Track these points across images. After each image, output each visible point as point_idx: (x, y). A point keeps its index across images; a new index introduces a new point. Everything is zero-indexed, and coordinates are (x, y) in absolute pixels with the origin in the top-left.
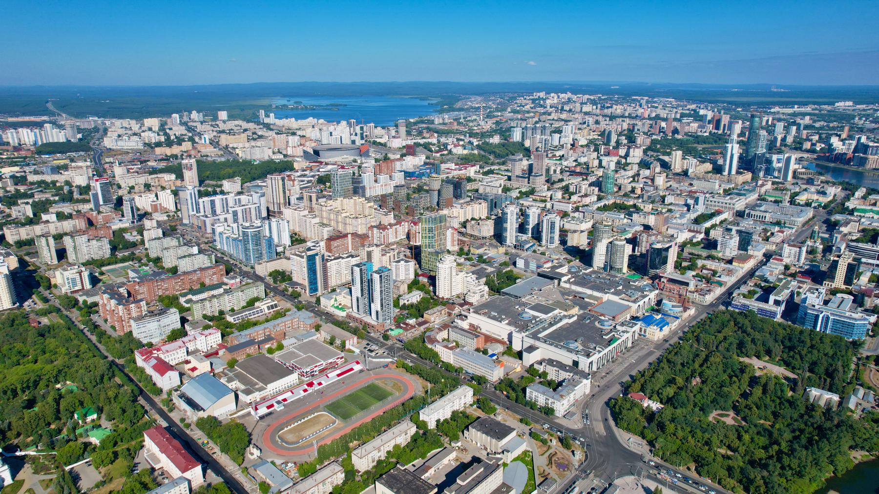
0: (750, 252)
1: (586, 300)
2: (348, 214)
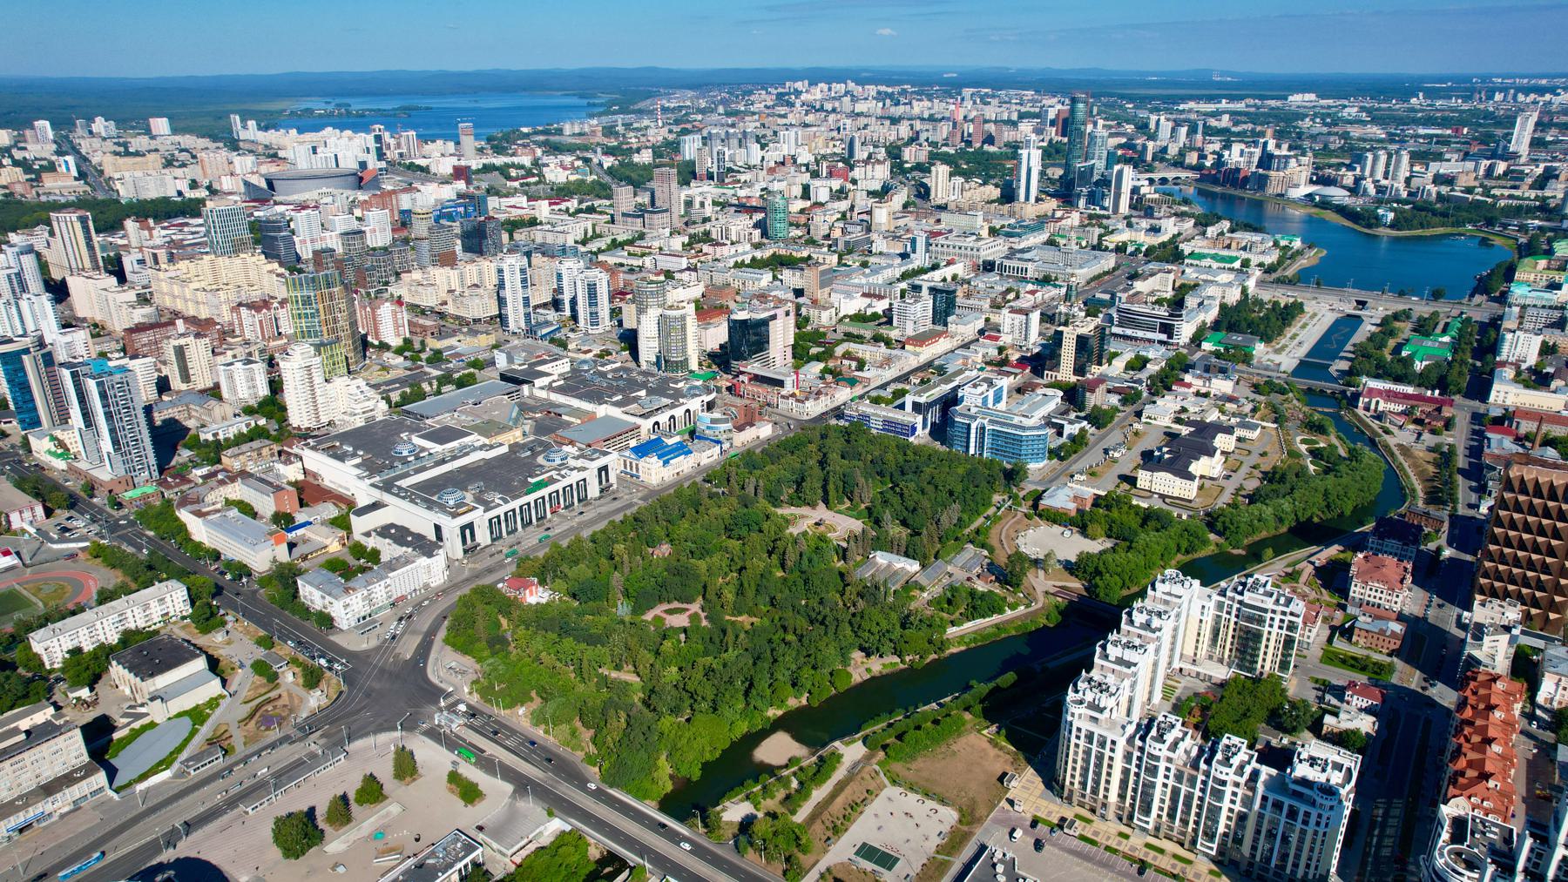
0: (952, 328)
1: (565, 417)
2: (203, 284)
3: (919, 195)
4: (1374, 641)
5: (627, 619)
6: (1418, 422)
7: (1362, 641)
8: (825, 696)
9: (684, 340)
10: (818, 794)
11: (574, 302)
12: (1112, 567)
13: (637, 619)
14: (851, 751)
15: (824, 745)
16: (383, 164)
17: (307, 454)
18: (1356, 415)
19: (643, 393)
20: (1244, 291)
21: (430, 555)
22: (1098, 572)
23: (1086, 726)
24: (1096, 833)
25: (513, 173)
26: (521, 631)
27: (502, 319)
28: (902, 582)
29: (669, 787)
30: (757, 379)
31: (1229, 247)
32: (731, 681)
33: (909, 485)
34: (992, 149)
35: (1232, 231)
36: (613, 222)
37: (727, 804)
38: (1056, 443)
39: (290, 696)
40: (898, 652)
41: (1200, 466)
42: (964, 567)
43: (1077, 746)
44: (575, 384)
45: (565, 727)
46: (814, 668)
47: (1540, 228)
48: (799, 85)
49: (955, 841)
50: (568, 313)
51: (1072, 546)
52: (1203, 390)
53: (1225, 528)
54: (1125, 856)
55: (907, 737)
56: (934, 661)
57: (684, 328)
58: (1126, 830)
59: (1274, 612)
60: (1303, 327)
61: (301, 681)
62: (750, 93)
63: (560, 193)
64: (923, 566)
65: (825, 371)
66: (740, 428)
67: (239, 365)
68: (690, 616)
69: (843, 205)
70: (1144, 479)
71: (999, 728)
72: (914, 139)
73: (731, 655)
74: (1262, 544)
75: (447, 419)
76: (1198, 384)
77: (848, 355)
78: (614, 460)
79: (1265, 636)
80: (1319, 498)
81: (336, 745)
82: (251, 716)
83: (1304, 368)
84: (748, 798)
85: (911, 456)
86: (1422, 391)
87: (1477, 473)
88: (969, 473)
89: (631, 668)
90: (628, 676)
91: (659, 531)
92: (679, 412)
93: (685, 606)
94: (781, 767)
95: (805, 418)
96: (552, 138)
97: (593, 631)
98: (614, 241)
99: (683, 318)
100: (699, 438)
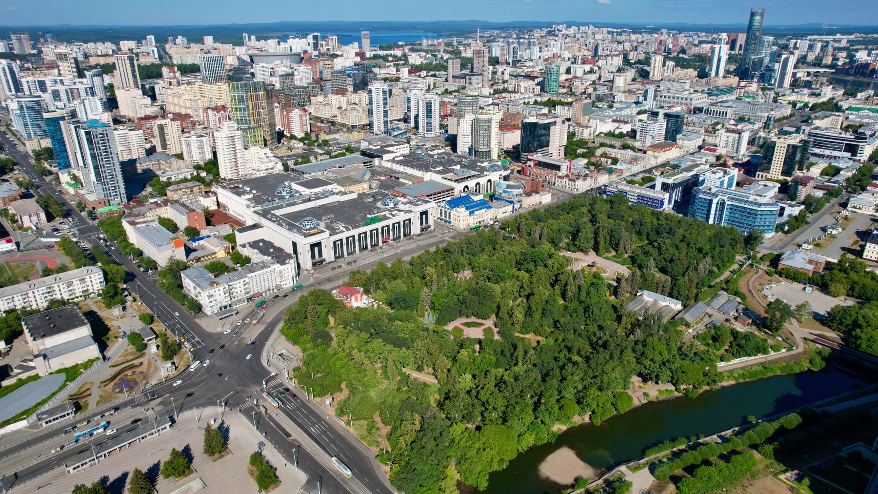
0: (679, 142)
1: (401, 180)
3: (641, 76)
5: (431, 327)
8: (608, 416)
9: (489, 137)
11: (417, 117)
15: (610, 468)
17: (220, 191)
19: (458, 167)
22: (856, 325)
25: (390, 59)
27: (370, 125)
30: (540, 164)
33: (667, 243)
36: (447, 80)
38: (779, 220)
39: (149, 364)
40: (675, 382)
42: (719, 309)
44: (410, 160)
46: (600, 389)
48: (560, 27)
50: (413, 124)
51: (823, 303)
56: (706, 392)
57: (489, 128)
61: (161, 353)
62: (532, 31)
63: (414, 70)
64: (685, 306)
65: (588, 164)
66: (528, 194)
67: (194, 138)
68: (484, 330)
69: (594, 77)
71: (799, 479)
73: (520, 369)
75: (319, 175)
77: (605, 155)
78: (432, 207)
82: (114, 377)
85: (663, 221)
88: (716, 235)
89: (431, 370)
90: (426, 377)
91: (463, 260)
92: (483, 181)
93: (480, 321)
95: (575, 193)
98: (446, 90)
99: (489, 121)
100: (497, 199)
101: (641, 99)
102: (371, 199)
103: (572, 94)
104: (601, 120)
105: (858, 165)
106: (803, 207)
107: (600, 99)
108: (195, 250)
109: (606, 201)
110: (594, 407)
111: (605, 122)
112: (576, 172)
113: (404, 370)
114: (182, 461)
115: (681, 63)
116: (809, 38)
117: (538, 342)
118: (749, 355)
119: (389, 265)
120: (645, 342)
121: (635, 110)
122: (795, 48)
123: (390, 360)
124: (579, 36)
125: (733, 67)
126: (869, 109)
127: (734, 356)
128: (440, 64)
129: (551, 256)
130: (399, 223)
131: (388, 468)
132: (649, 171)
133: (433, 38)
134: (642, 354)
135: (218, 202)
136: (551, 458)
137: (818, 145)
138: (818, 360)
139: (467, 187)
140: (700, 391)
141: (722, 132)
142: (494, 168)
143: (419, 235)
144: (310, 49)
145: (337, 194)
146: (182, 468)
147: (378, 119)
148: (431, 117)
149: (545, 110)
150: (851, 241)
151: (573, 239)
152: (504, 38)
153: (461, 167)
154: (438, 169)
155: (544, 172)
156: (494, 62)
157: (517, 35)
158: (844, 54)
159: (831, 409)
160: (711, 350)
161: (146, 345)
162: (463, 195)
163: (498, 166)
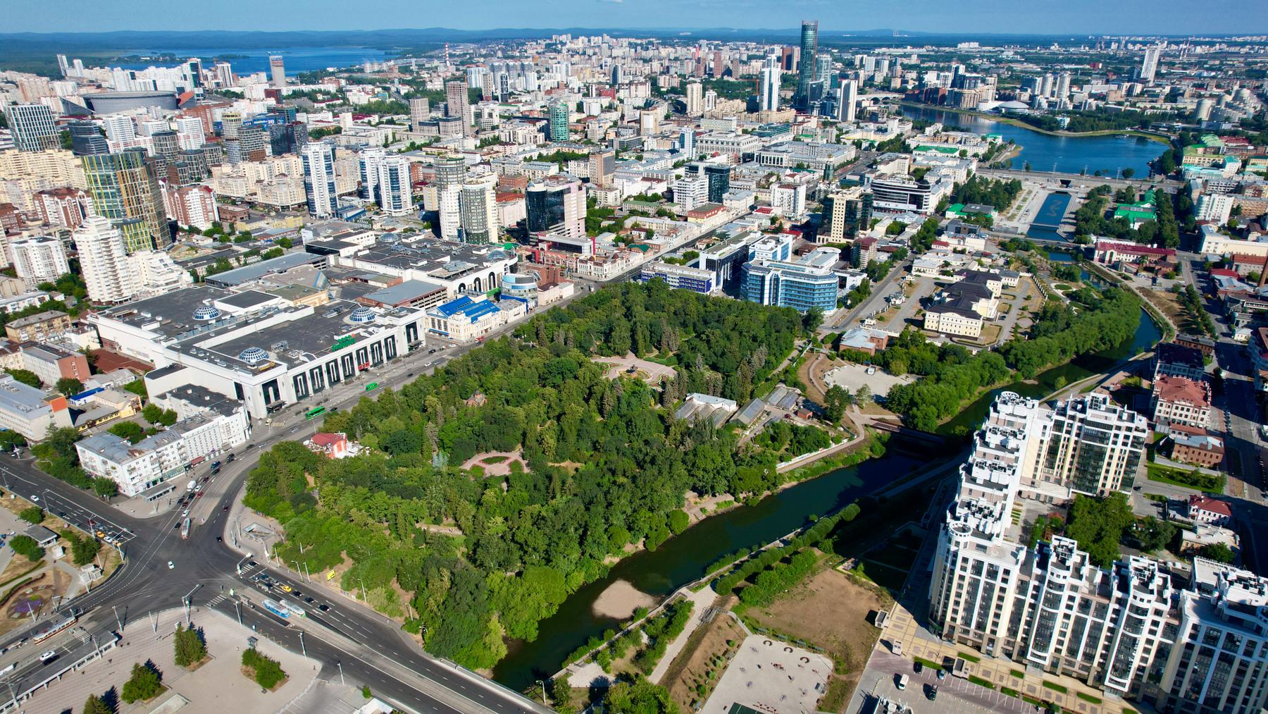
0: (726, 203)
1: (371, 283)
3: (677, 110)
4: (1195, 456)
5: (444, 469)
6: (1147, 269)
7: (1182, 457)
8: (663, 539)
9: (484, 213)
10: (673, 648)
11: (377, 188)
12: (928, 398)
13: (455, 469)
14: (701, 598)
15: (670, 593)
16: (200, 91)
17: (102, 322)
18: (1094, 266)
19: (447, 259)
20: (969, 173)
21: (229, 413)
22: (913, 403)
23: (974, 555)
24: (987, 673)
25: (320, 97)
26: (328, 487)
27: (309, 204)
28: (722, 421)
29: (504, 652)
30: (556, 246)
31: (947, 141)
32: (564, 529)
33: (715, 333)
34: (731, 79)
35: (945, 130)
36: (411, 130)
37: (571, 666)
38: (842, 293)
39: (57, 574)
41: (984, 307)
42: (778, 404)
43: (962, 578)
44: (379, 253)
45: (380, 591)
46: (651, 509)
47: (1184, 129)
48: (563, 38)
49: (836, 694)
50: (372, 199)
51: (881, 383)
52: (960, 248)
53: (1017, 361)
54: (1027, 698)
55: (761, 578)
57: (483, 202)
58: (1019, 668)
59: (1119, 428)
60: (1024, 200)
61: (71, 556)
62: (524, 44)
63: (361, 113)
64: (740, 406)
65: (618, 240)
66: (544, 288)
67: (33, 243)
68: (510, 465)
69: (615, 116)
70: (932, 320)
71: (855, 568)
72: (666, 71)
73: (559, 501)
74: (1058, 371)
75: (251, 286)
76: (954, 243)
77: (636, 227)
78: (420, 317)
79: (1108, 453)
80: (1095, 331)
81: (109, 630)
83: (1034, 230)
84: (594, 657)
85: (711, 308)
86: (1141, 245)
87: (1223, 308)
88: (770, 319)
89: (451, 521)
90: (447, 529)
91: (472, 382)
92: (483, 275)
93: (504, 454)
94: (626, 620)
95: (604, 279)
96: (354, 75)
97: (408, 483)
98: (413, 144)
99: (482, 192)
100: (505, 298)
101: (677, 146)
102: (335, 314)
103: (589, 143)
104: (629, 179)
105: (923, 219)
106: (865, 275)
107: (625, 147)
108: (82, 412)
109: (641, 288)
110: (646, 531)
111: (634, 182)
112: (602, 252)
113: (418, 526)
114: (150, 677)
115: (726, 91)
116: (877, 51)
117: (577, 470)
118: (810, 451)
119: (375, 399)
120: (700, 456)
121: (670, 161)
122: (862, 66)
123: (400, 515)
124: (590, 52)
125: (789, 94)
126: (937, 149)
127: (795, 455)
128: (396, 103)
129: (581, 365)
130: (379, 343)
131: (419, 636)
132: (692, 244)
133: (378, 58)
134: (693, 465)
135: (100, 338)
136: (605, 594)
137: (882, 196)
138: (878, 446)
139: (463, 285)
140: (762, 497)
141: (774, 187)
142: (496, 257)
143: (408, 356)
144: (189, 86)
145: (285, 310)
146: (151, 687)
147: (322, 196)
148: (398, 189)
149: (554, 169)
150: (915, 311)
151: (607, 341)
152: (485, 56)
153: (452, 259)
154: (420, 264)
155: (561, 256)
156: (476, 96)
157: (503, 51)
158: (914, 75)
159: (888, 495)
160: (769, 451)
161: (43, 550)
162: (460, 296)
163: (500, 253)
